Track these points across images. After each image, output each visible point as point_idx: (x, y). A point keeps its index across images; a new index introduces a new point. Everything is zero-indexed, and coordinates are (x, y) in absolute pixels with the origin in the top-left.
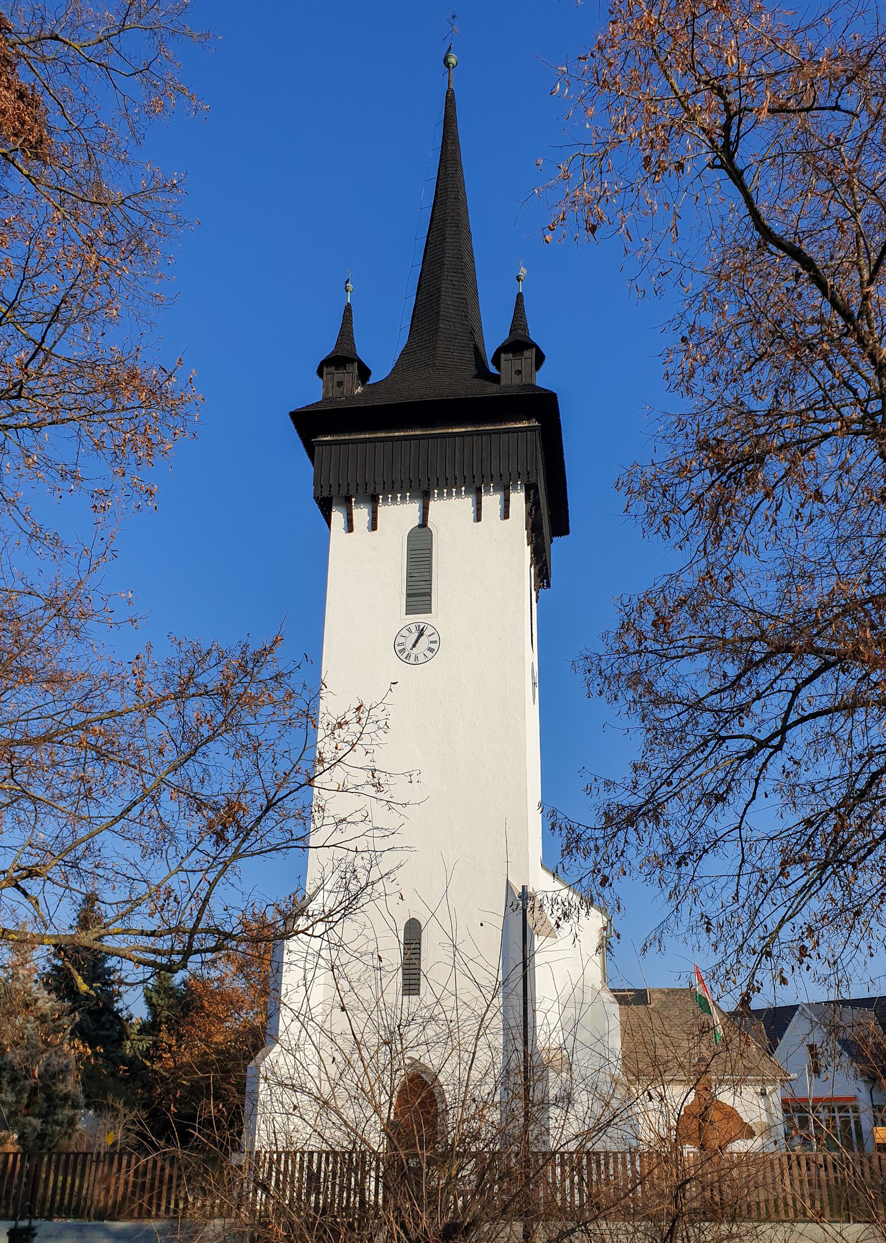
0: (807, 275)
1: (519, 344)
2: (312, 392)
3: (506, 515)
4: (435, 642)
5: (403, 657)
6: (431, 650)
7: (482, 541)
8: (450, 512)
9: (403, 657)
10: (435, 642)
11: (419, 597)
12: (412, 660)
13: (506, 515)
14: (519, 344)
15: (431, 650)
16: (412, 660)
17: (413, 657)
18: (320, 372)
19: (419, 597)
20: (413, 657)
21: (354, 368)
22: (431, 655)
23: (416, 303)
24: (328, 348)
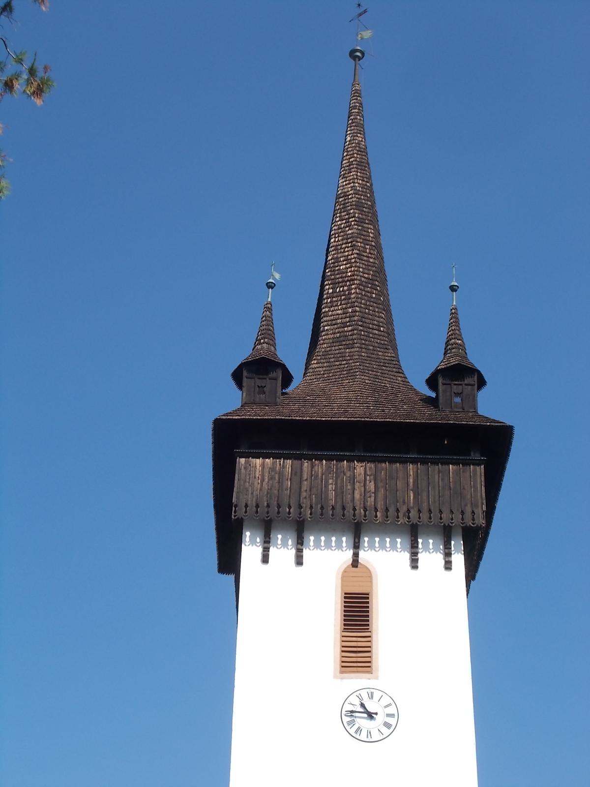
0: (398, 464)
1: (458, 374)
2: (229, 400)
3: (448, 566)
4: (392, 716)
5: (352, 731)
6: (387, 725)
7: (424, 594)
8: (385, 559)
9: (352, 731)
10: (392, 716)
11: (356, 655)
12: (363, 736)
13: (448, 566)
14: (458, 374)
15: (387, 725)
16: (363, 736)
17: (364, 733)
18: (237, 377)
19: (356, 655)
20: (364, 733)
21: (279, 374)
22: (389, 731)
23: (308, 357)
24: (243, 353)
